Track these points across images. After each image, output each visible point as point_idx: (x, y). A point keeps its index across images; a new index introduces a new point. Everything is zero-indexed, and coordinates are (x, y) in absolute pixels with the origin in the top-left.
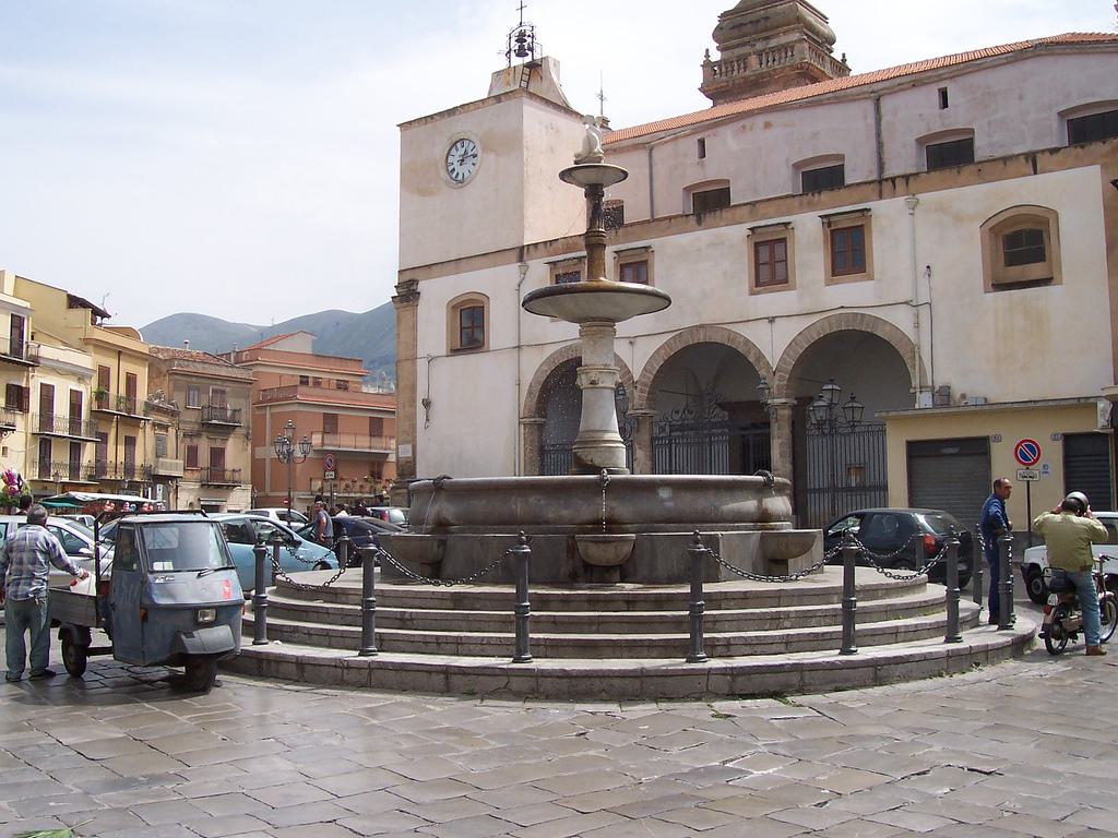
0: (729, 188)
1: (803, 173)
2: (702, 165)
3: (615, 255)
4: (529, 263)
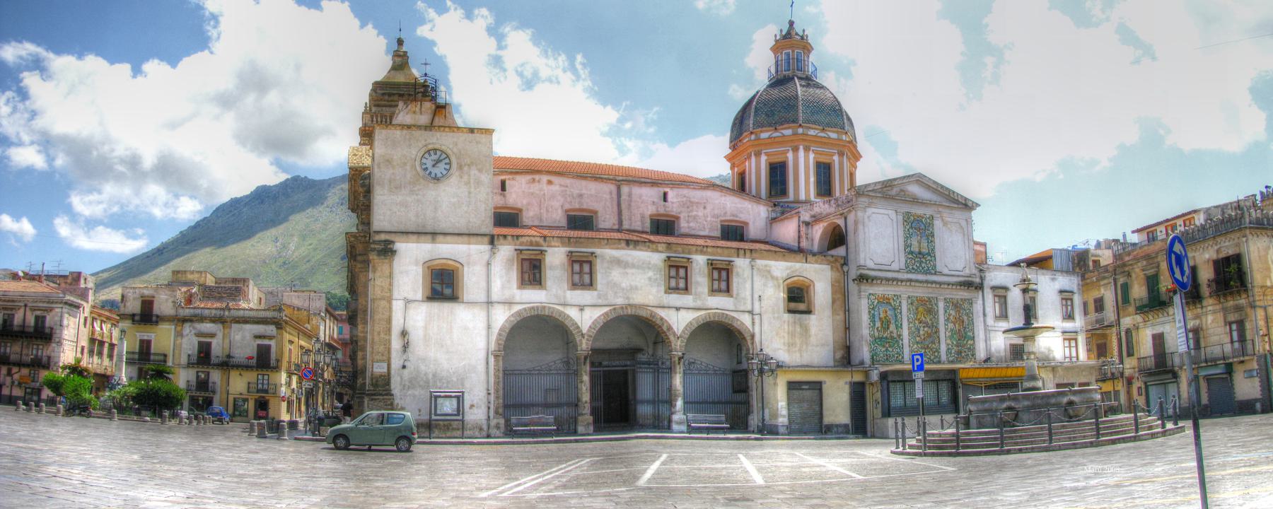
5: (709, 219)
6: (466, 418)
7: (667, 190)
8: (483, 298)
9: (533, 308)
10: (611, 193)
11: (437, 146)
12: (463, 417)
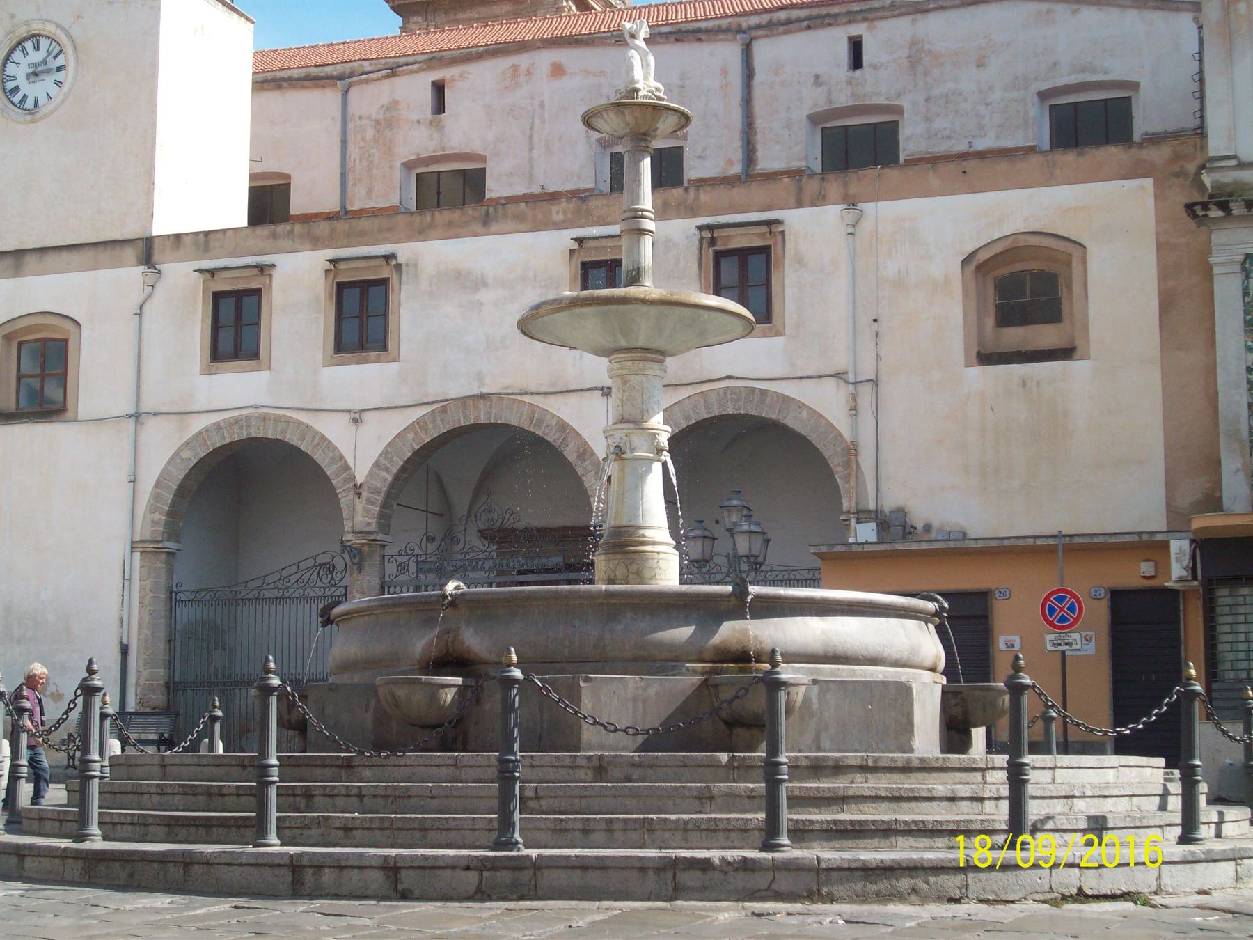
0: (484, 169)
2: (435, 125)
3: (329, 266)
5: (997, 95)
7: (856, 30)
8: (148, 404)
9: (237, 421)
10: (725, 73)
11: (36, 28)
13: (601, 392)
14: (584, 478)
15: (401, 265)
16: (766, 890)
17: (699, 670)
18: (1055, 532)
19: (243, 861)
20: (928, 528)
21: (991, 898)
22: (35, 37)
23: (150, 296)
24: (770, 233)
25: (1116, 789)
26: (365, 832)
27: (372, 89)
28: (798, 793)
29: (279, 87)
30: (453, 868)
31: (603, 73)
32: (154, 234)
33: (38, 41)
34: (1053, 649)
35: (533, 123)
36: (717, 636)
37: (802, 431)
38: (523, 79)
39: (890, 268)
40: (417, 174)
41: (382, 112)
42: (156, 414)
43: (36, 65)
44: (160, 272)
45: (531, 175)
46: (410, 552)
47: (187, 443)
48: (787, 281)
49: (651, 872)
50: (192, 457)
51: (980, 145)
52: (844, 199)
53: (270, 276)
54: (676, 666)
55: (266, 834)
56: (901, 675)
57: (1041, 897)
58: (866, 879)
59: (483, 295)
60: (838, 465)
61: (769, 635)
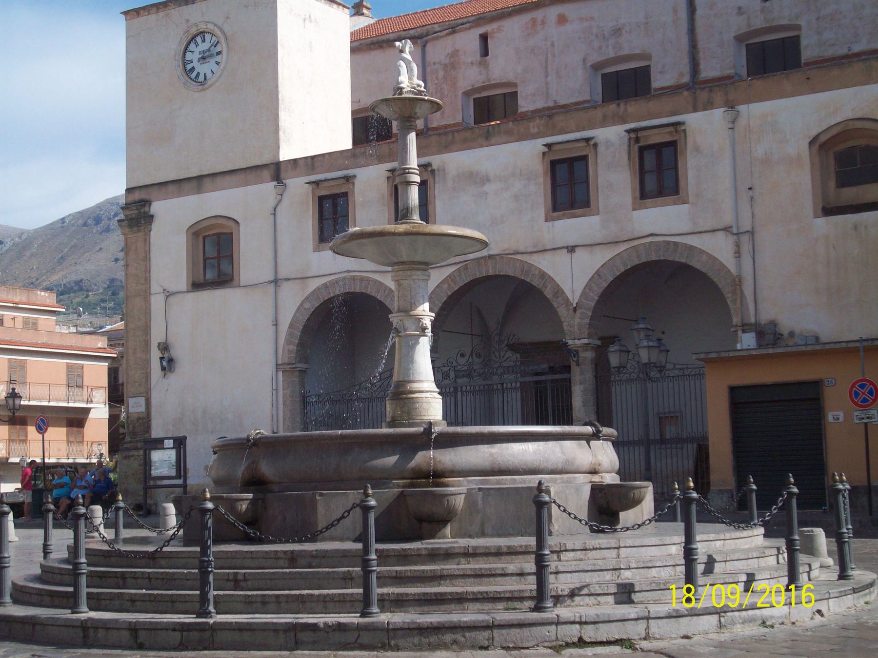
0: (517, 92)
1: (603, 75)
3: (389, 174)
4: (288, 182)
6: (188, 482)
8: (282, 274)
11: (202, 27)
12: (185, 480)
13: (566, 250)
14: (558, 310)
15: (434, 170)
16: (353, 643)
17: (401, 484)
18: (857, 338)
19: (59, 623)
20: (792, 334)
21: (511, 646)
22: (202, 33)
23: (280, 201)
24: (676, 132)
25: (659, 562)
26: (142, 603)
27: (440, 43)
28: (409, 574)
29: (381, 47)
30: (167, 630)
31: (592, 19)
32: (281, 159)
33: (204, 36)
34: (858, 421)
35: (547, 58)
36: (413, 462)
37: (704, 269)
38: (539, 27)
39: (760, 151)
40: (474, 99)
41: (448, 59)
42: (287, 280)
43: (204, 52)
44: (285, 185)
45: (547, 94)
46: (450, 364)
47: (307, 298)
48: (689, 165)
49: (281, 632)
50: (311, 306)
51: (856, 49)
52: (726, 103)
53: (353, 184)
54: (386, 482)
55: (79, 605)
56: (556, 480)
57: (550, 645)
58: (421, 635)
59: (487, 188)
60: (728, 292)
61: (450, 460)
